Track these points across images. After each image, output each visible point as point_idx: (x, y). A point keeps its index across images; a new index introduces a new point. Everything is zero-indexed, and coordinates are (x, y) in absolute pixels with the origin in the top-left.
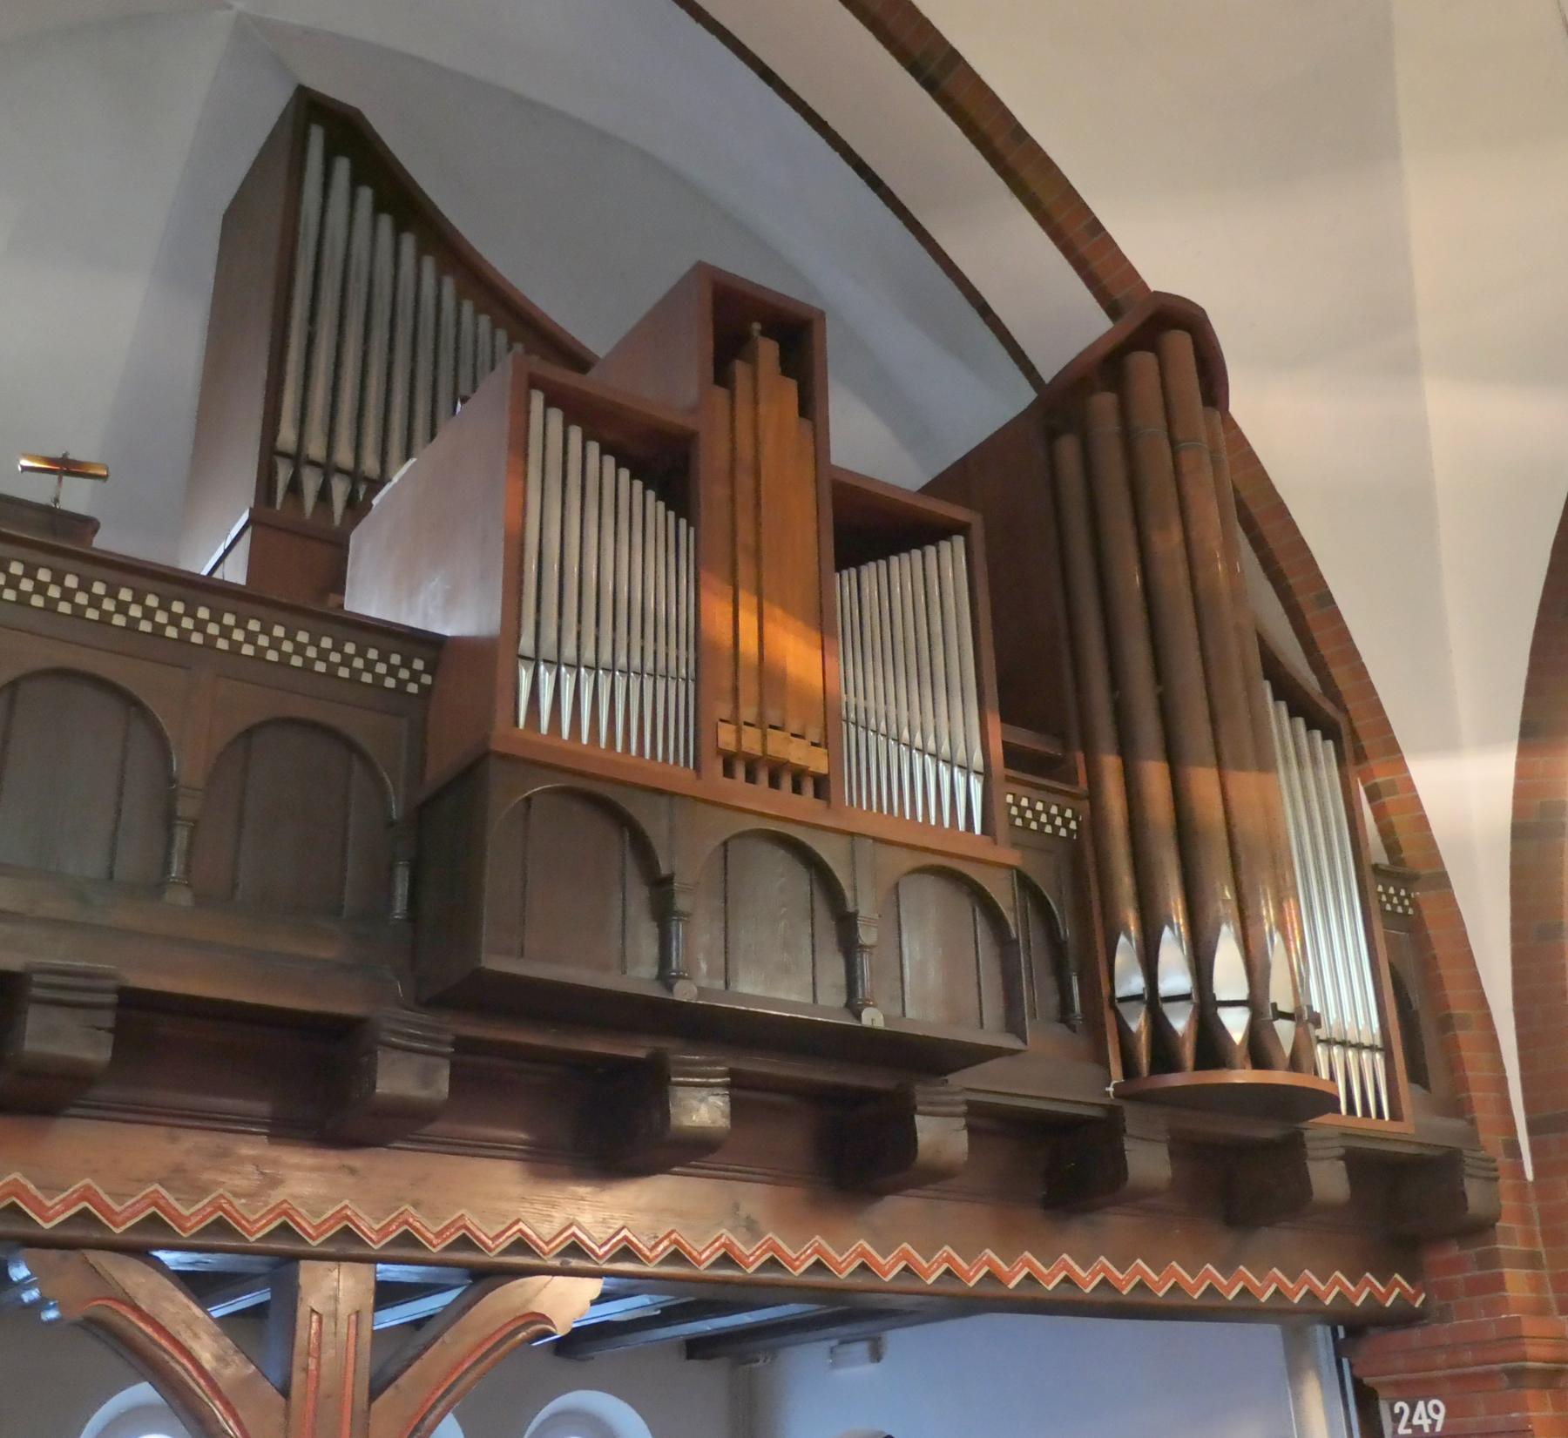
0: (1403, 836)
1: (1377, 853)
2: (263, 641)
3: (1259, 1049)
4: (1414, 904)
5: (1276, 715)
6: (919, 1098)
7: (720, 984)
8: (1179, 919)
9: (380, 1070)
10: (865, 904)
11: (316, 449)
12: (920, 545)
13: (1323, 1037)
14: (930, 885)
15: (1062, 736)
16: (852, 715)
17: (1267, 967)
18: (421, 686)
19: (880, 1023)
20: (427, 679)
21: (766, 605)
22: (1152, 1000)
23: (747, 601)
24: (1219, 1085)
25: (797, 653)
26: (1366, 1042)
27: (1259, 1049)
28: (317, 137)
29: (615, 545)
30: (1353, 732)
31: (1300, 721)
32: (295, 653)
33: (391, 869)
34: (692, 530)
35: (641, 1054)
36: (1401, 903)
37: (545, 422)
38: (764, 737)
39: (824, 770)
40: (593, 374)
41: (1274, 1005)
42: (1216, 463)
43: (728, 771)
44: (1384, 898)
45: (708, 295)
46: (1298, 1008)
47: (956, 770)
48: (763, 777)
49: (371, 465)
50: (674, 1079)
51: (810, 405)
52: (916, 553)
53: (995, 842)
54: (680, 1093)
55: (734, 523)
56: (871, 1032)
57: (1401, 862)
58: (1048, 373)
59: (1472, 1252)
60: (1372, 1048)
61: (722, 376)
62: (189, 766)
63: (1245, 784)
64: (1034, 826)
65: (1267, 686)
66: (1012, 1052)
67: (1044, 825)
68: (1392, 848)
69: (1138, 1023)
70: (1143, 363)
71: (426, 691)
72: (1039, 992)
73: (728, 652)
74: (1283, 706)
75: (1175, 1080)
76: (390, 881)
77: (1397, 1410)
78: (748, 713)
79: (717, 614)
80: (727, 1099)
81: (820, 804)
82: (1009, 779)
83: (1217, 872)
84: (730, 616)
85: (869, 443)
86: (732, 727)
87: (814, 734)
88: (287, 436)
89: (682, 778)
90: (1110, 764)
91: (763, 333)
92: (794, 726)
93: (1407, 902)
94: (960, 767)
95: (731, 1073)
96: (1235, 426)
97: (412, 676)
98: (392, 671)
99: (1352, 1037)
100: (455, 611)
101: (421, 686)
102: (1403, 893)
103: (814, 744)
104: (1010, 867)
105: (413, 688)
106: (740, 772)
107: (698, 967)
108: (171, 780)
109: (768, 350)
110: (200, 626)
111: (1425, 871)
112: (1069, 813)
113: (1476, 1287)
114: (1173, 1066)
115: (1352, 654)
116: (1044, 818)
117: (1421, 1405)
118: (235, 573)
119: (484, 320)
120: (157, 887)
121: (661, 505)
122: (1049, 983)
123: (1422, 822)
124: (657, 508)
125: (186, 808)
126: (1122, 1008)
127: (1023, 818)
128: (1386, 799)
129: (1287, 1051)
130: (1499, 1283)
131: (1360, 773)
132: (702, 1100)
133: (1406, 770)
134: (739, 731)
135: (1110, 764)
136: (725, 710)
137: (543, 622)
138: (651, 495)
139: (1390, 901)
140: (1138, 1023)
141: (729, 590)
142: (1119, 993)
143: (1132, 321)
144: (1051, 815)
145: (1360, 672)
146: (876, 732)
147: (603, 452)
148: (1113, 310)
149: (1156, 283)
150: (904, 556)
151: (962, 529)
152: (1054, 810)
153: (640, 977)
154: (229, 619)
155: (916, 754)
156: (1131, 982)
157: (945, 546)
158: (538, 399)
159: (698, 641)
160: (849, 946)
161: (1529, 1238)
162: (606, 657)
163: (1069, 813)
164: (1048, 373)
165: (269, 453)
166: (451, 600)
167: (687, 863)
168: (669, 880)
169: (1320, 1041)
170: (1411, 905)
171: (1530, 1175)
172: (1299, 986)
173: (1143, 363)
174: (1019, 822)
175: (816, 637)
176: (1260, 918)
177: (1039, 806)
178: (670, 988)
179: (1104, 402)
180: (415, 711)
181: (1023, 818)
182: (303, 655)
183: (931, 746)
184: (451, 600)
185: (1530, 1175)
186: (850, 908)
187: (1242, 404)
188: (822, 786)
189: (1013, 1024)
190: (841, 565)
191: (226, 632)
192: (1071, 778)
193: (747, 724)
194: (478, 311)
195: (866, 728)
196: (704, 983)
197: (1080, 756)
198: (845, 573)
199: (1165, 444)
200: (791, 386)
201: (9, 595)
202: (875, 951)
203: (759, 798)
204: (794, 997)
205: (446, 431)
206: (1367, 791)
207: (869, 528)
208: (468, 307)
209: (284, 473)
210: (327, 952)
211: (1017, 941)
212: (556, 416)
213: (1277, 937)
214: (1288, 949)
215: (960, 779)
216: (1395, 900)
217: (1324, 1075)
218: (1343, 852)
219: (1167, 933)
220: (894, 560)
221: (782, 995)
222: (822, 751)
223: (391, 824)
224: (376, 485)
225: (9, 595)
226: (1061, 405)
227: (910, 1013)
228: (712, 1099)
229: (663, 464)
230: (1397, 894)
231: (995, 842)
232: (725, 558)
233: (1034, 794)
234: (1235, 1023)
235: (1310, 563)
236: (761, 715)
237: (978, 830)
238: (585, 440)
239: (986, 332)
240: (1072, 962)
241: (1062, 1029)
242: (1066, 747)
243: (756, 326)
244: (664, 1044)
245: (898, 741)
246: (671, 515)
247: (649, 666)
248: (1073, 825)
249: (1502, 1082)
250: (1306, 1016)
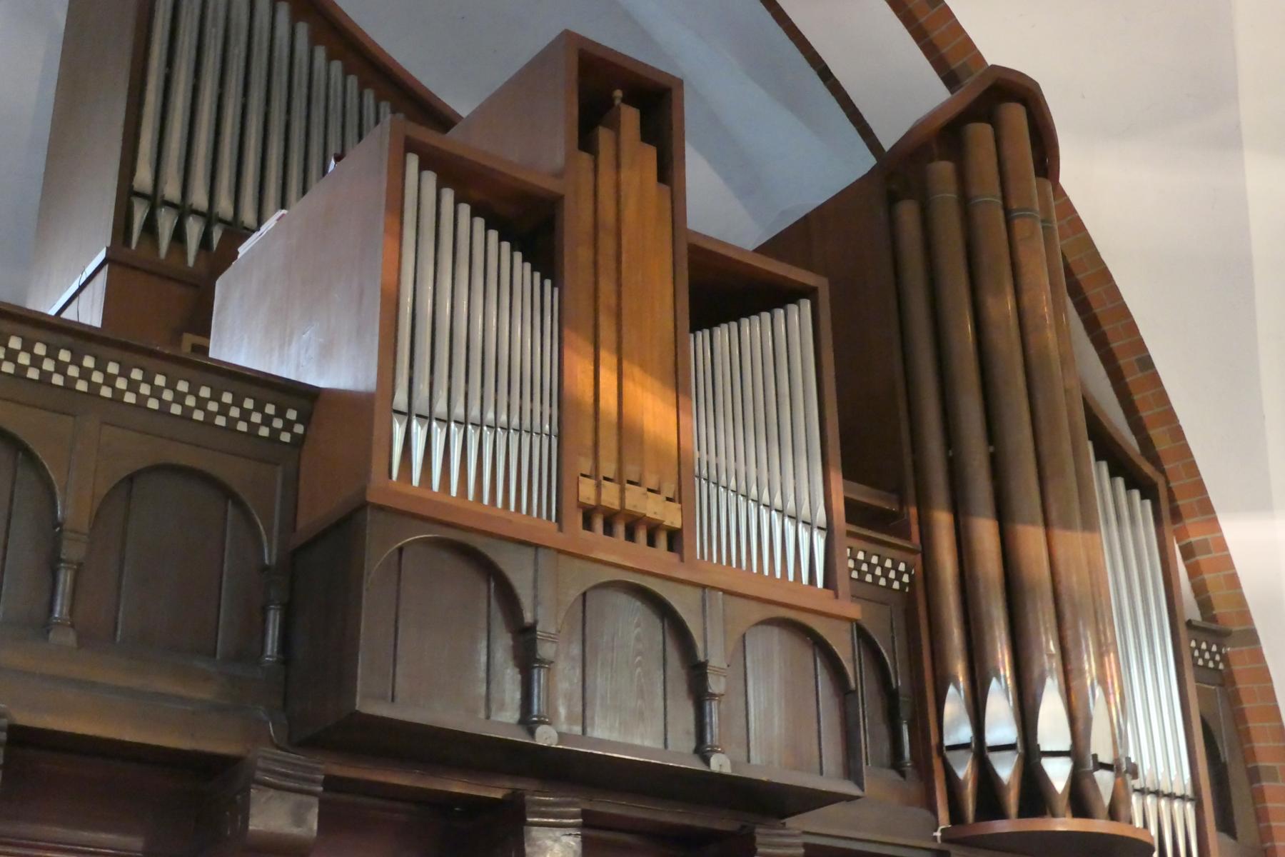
0: (1217, 594)
1: (1191, 610)
2: (145, 389)
3: (1080, 801)
4: (1225, 658)
5: (1099, 472)
6: (759, 839)
7: (577, 729)
8: (1006, 670)
9: (253, 811)
10: (715, 654)
11: (171, 191)
12: (769, 309)
13: (1137, 787)
14: (775, 634)
15: (898, 491)
16: (704, 472)
17: (1088, 720)
18: (294, 436)
19: (727, 770)
20: (299, 429)
21: (625, 365)
22: (980, 750)
23: (608, 360)
24: (1042, 832)
25: (653, 410)
26: (1179, 792)
27: (1080, 801)
29: (482, 300)
30: (1170, 490)
31: (1120, 482)
32: (175, 401)
33: (264, 611)
34: (556, 290)
35: (498, 795)
36: (1213, 659)
37: (421, 185)
38: (622, 491)
39: (678, 524)
40: (453, 132)
41: (1095, 756)
42: (1048, 231)
43: (588, 524)
44: (1196, 653)
45: (574, 60)
46: (1117, 760)
47: (800, 525)
48: (620, 529)
49: (248, 217)
50: (530, 820)
51: (668, 170)
52: (766, 316)
53: (837, 596)
54: (536, 832)
55: (596, 283)
56: (713, 774)
57: (1214, 619)
58: (888, 141)
60: (1183, 798)
61: (587, 142)
62: (73, 508)
63: (1071, 543)
64: (869, 578)
65: (1090, 445)
66: (850, 798)
67: (878, 578)
68: (1205, 604)
69: (964, 770)
70: (980, 133)
71: (298, 441)
72: (872, 739)
73: (590, 410)
74: (1104, 466)
75: (1001, 826)
76: (265, 621)
78: (608, 468)
79: (579, 370)
80: (579, 839)
81: (673, 557)
82: (850, 534)
83: (1032, 622)
84: (591, 374)
85: (727, 207)
86: (591, 482)
87: (669, 489)
88: (143, 178)
89: (547, 532)
90: (943, 520)
91: (624, 100)
92: (651, 481)
93: (1218, 658)
94: (790, 517)
95: (584, 814)
96: (1064, 194)
97: (260, 419)
98: (267, 420)
99: (1166, 788)
100: (331, 363)
101: (294, 436)
102: (1214, 648)
103: (668, 499)
104: (851, 620)
105: (286, 437)
106: (598, 524)
107: (556, 711)
108: (57, 524)
109: (630, 117)
110: (180, 398)
111: (1236, 628)
112: (902, 567)
114: (1001, 814)
115: (1169, 416)
116: (878, 571)
118: (90, 313)
119: (337, 66)
120: (45, 625)
121: (528, 266)
122: (883, 731)
123: (1233, 581)
124: (523, 270)
125: (72, 551)
126: (950, 756)
127: (859, 571)
128: (1201, 558)
129: (1107, 801)
131: (1175, 532)
132: (556, 840)
133: (1220, 530)
134: (598, 487)
135: (943, 520)
136: (586, 465)
137: (416, 380)
138: (518, 256)
139: (1201, 655)
140: (964, 770)
141: (591, 349)
142: (948, 742)
143: (971, 90)
144: (893, 570)
145: (1177, 433)
146: (726, 488)
147: (473, 214)
148: (951, 80)
149: (992, 57)
150: (755, 318)
151: (808, 292)
152: (888, 564)
153: (503, 720)
154: (113, 368)
155: (764, 511)
156: (958, 731)
157: (793, 308)
158: (413, 161)
159: (562, 399)
160: (699, 694)
162: (475, 413)
163: (902, 567)
164: (888, 141)
165: (126, 194)
166: (326, 352)
167: (547, 612)
168: (531, 629)
169: (1136, 790)
170: (1222, 660)
172: (1118, 740)
173: (980, 133)
174: (855, 575)
175: (671, 396)
176: (1081, 672)
177: (875, 560)
178: (532, 733)
179: (943, 170)
180: (286, 458)
181: (859, 571)
182: (182, 404)
183: (778, 502)
184: (326, 352)
186: (701, 657)
187: (1075, 173)
188: (675, 539)
189: (852, 771)
190: (694, 328)
191: (109, 380)
192: (904, 533)
193: (606, 479)
194: (330, 58)
195: (717, 484)
196: (564, 728)
197: (913, 511)
198: (699, 334)
199: (1001, 213)
200: (651, 153)
201: (8, 368)
202: (723, 699)
203: (616, 551)
204: (648, 743)
205: (316, 188)
206: (1181, 548)
207: (722, 291)
208: (320, 53)
209: (140, 213)
210: (205, 693)
211: (855, 692)
212: (430, 178)
213: (1098, 691)
214: (1108, 703)
215: (804, 535)
216: (1207, 656)
217: (1138, 823)
219: (994, 684)
220: (745, 322)
221: (637, 741)
222: (676, 506)
223: (265, 569)
224: (246, 233)
225: (8, 368)
226: (902, 171)
227: (756, 758)
228: (565, 839)
229: (530, 226)
230: (1209, 650)
231: (837, 596)
232: (585, 317)
233: (870, 547)
234: (1058, 773)
235: (1132, 328)
236: (620, 470)
237: (820, 583)
238: (457, 202)
239: (812, 74)
240: (905, 711)
241: (893, 775)
242: (902, 502)
243: (618, 94)
244: (520, 785)
245: (746, 497)
246: (537, 275)
247: (515, 422)
248: (906, 579)
250: (1124, 767)
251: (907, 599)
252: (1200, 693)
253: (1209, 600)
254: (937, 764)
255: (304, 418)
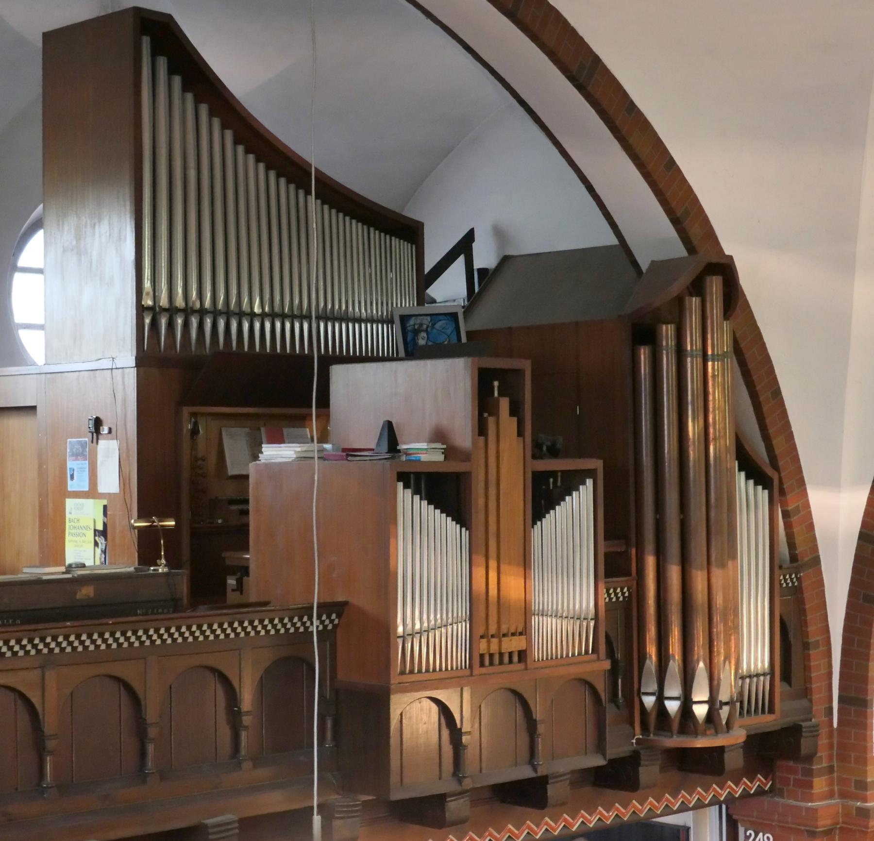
0: (798, 540)
20: (336, 622)
28: (146, 42)
59: (800, 766)
73: (483, 597)
74: (743, 474)
77: (748, 834)
90: (650, 562)
113: (800, 784)
117: (761, 835)
123: (811, 527)
130: (810, 785)
134: (489, 642)
135: (650, 562)
142: (642, 691)
161: (831, 758)
171: (835, 725)
185: (835, 725)
197: (634, 551)
206: (782, 511)
218: (764, 585)
234: (700, 711)
248: (627, 594)
249: (830, 675)
251: (628, 602)
252: (782, 603)
253: (795, 544)
254: (636, 700)
255: (339, 616)
